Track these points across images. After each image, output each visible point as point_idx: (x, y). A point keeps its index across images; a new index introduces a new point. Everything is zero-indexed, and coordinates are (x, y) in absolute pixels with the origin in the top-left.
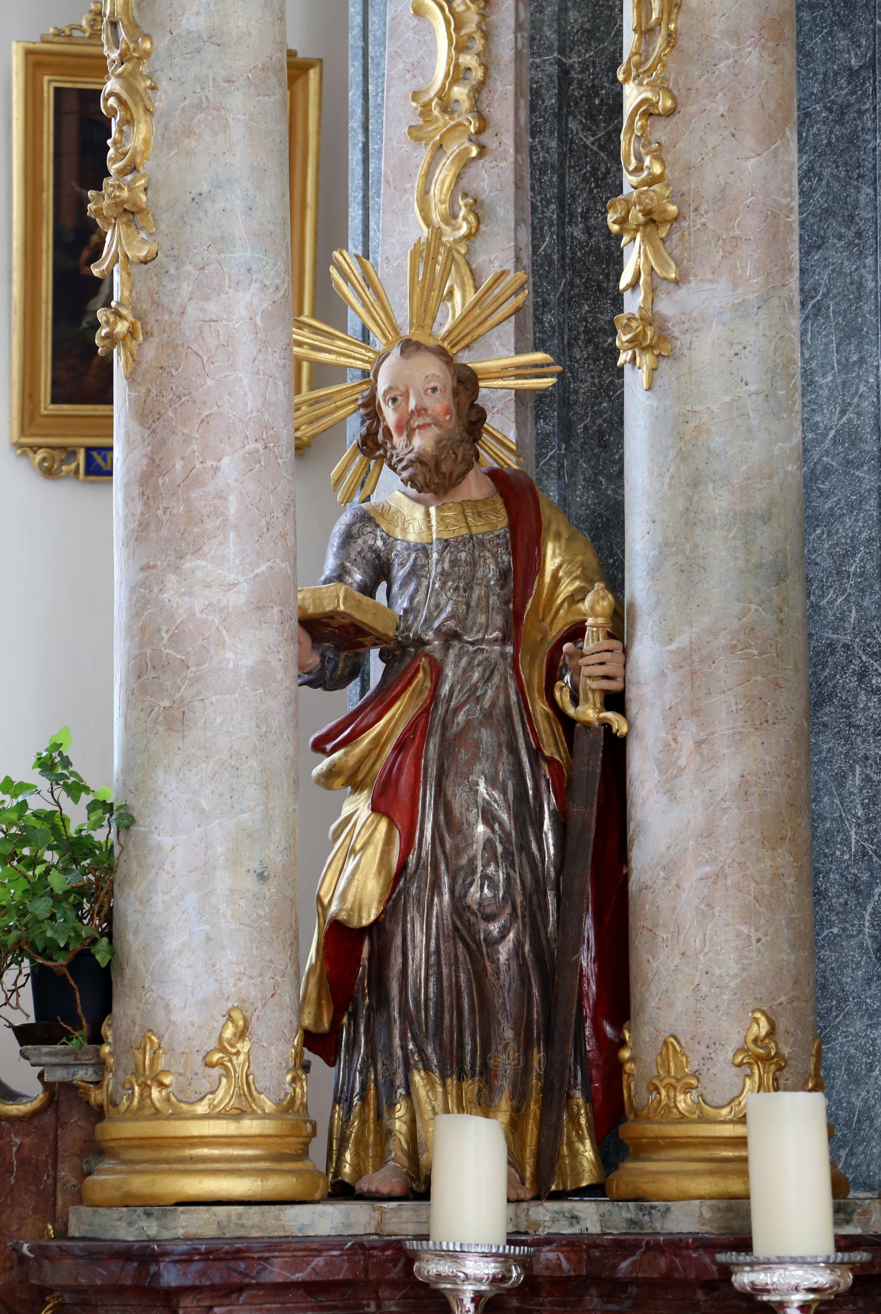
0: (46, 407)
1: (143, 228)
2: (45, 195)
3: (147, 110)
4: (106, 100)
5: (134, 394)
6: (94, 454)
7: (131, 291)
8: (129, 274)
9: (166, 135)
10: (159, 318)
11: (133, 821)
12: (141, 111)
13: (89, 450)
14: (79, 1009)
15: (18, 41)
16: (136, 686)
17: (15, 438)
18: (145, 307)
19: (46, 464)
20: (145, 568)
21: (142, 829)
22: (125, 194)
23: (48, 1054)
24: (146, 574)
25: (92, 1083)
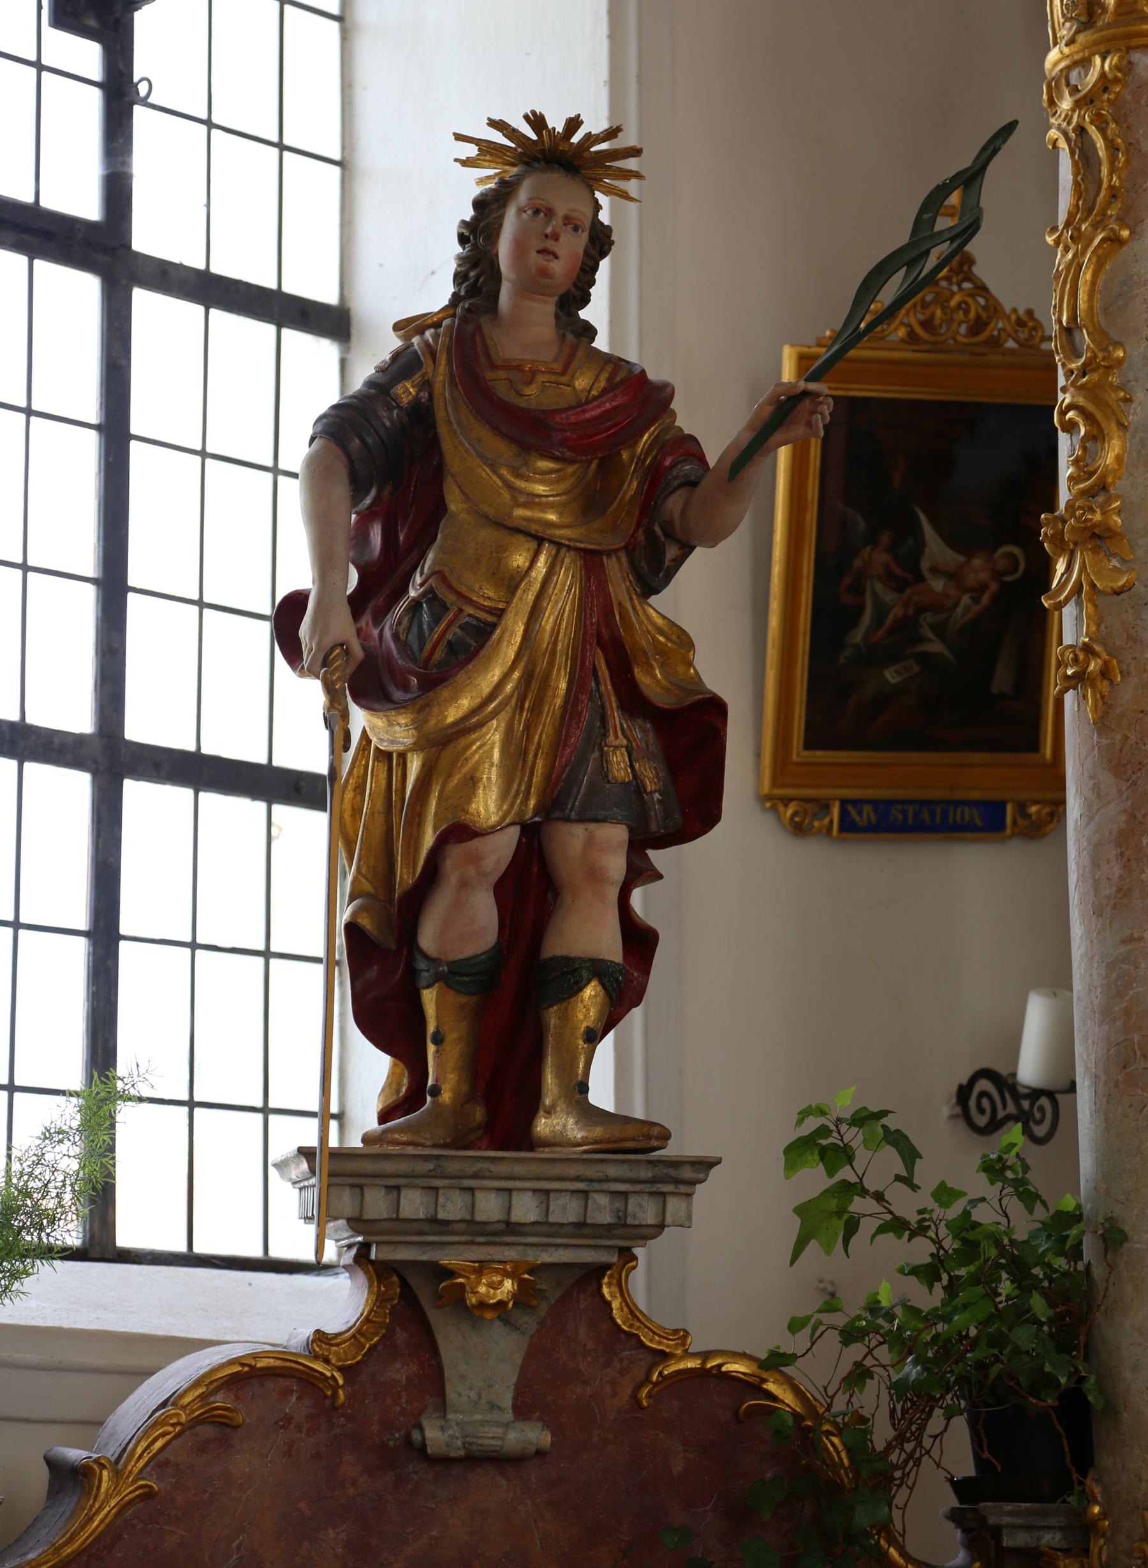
0: (797, 752)
1: (1114, 555)
2: (808, 515)
3: (1120, 425)
4: (1063, 413)
5: (1104, 742)
6: (850, 808)
7: (1098, 626)
8: (1096, 606)
9: (1143, 452)
10: (1137, 655)
11: (1124, 1237)
12: (1114, 426)
13: (844, 802)
14: (1068, 1460)
15: (792, 346)
16: (1121, 1078)
17: (766, 787)
18: (1118, 643)
19: (797, 819)
20: (1128, 940)
21: (1138, 1246)
22: (1098, 517)
23: (1010, 1514)
24: (1129, 947)
25: (1060, 1550)
